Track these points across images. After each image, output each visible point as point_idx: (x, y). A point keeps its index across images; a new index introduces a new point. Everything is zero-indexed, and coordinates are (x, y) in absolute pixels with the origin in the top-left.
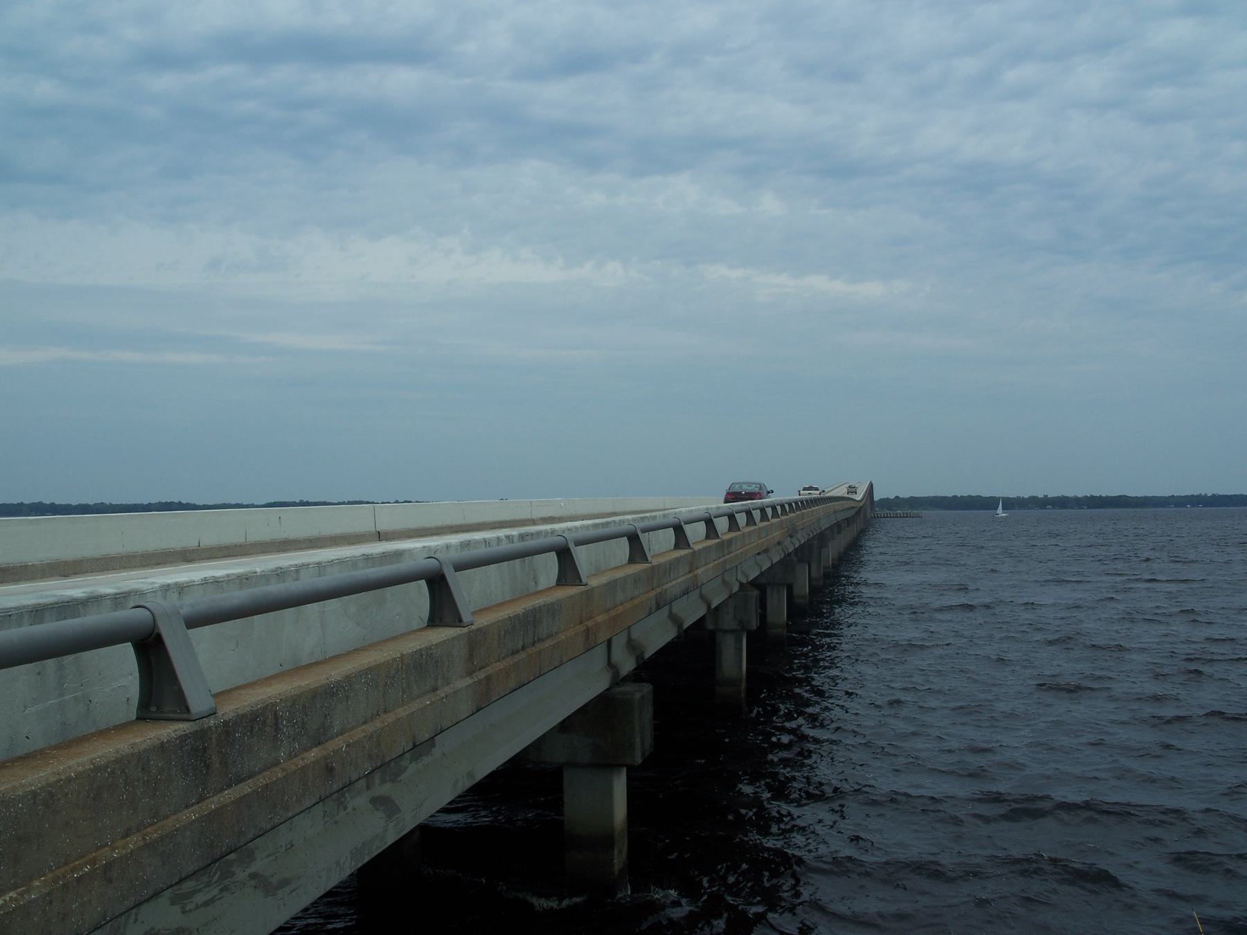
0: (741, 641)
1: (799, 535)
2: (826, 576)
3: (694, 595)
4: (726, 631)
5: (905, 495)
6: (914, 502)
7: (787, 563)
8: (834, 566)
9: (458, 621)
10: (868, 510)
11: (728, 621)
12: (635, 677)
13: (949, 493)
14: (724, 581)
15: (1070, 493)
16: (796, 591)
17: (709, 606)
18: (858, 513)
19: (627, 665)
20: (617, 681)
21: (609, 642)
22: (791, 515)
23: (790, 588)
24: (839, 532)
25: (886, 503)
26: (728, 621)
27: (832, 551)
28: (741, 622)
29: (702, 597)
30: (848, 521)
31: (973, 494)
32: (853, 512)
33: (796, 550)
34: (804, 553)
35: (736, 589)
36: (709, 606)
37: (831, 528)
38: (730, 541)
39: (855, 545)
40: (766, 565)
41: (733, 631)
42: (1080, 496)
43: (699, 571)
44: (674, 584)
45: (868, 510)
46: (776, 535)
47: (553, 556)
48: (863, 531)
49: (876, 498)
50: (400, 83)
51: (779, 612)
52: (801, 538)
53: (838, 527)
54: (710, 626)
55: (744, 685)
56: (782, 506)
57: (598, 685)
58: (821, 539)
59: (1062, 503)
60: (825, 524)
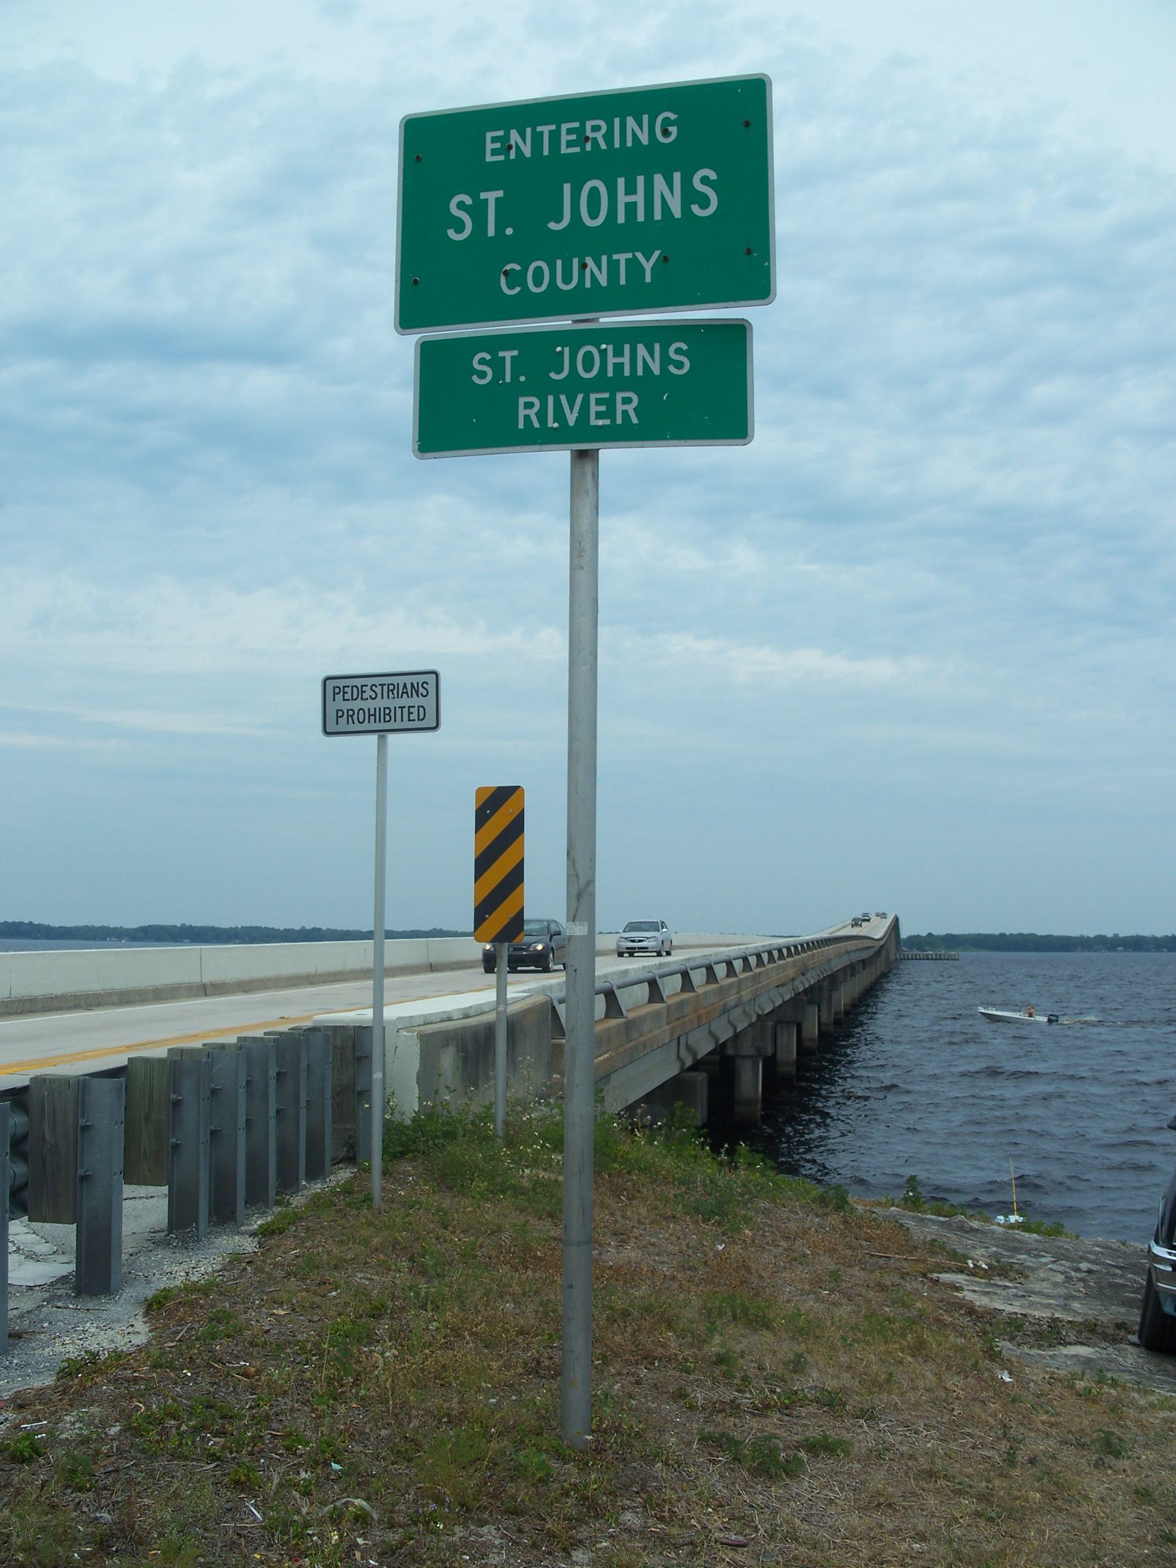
0: (757, 1073)
1: (809, 975)
2: (837, 1022)
3: (790, 986)
4: (744, 1057)
5: (940, 931)
6: (952, 941)
7: (798, 1002)
8: (847, 1013)
9: (662, 1000)
10: (893, 950)
11: (747, 1048)
12: (695, 1067)
13: (996, 931)
14: (744, 1012)
15: (1146, 932)
16: (805, 1034)
17: (717, 1041)
18: (879, 952)
19: (689, 1062)
20: (684, 1070)
21: (679, 1038)
22: (804, 955)
23: (799, 1027)
24: (853, 975)
25: (917, 942)
26: (747, 1048)
27: (844, 996)
28: (757, 1049)
29: (711, 1033)
30: (864, 963)
31: (1026, 932)
32: (871, 952)
33: (805, 990)
34: (814, 995)
35: (754, 1019)
36: (717, 1041)
37: (844, 970)
38: (759, 974)
39: (872, 992)
40: (779, 1002)
41: (750, 1057)
42: (1158, 935)
43: (743, 993)
44: (732, 999)
45: (893, 950)
46: (791, 972)
47: (704, 970)
48: (885, 976)
49: (904, 934)
50: (259, 388)
51: (788, 1051)
52: (811, 979)
53: (851, 970)
54: (730, 1052)
55: (759, 1106)
56: (802, 945)
57: (673, 1071)
58: (833, 980)
59: (1136, 944)
60: (837, 965)
